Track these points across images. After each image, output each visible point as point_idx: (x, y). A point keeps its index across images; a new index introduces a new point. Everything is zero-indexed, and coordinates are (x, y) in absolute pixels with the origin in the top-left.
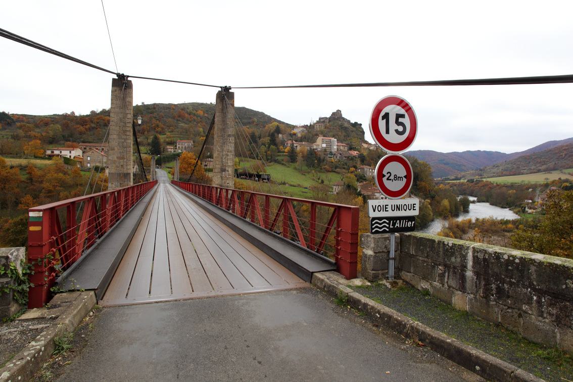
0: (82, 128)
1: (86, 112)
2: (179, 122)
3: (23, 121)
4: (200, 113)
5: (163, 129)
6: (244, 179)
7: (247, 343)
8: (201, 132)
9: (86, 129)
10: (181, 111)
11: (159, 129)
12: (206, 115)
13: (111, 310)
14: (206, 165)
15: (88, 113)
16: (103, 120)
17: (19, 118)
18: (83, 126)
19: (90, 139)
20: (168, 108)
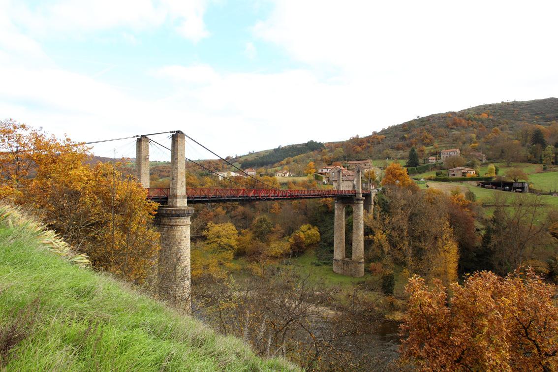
0: (359, 149)
1: (369, 133)
2: (453, 130)
3: (523, 105)
4: (484, 116)
5: (431, 140)
6: (489, 188)
7: (67, 137)
8: (473, 138)
9: (362, 149)
10: (457, 118)
11: (427, 141)
12: (491, 117)
13: (89, 146)
14: (454, 175)
15: (370, 134)
16: (377, 139)
17: (329, 145)
18: (360, 146)
19: (363, 157)
20: (445, 117)
